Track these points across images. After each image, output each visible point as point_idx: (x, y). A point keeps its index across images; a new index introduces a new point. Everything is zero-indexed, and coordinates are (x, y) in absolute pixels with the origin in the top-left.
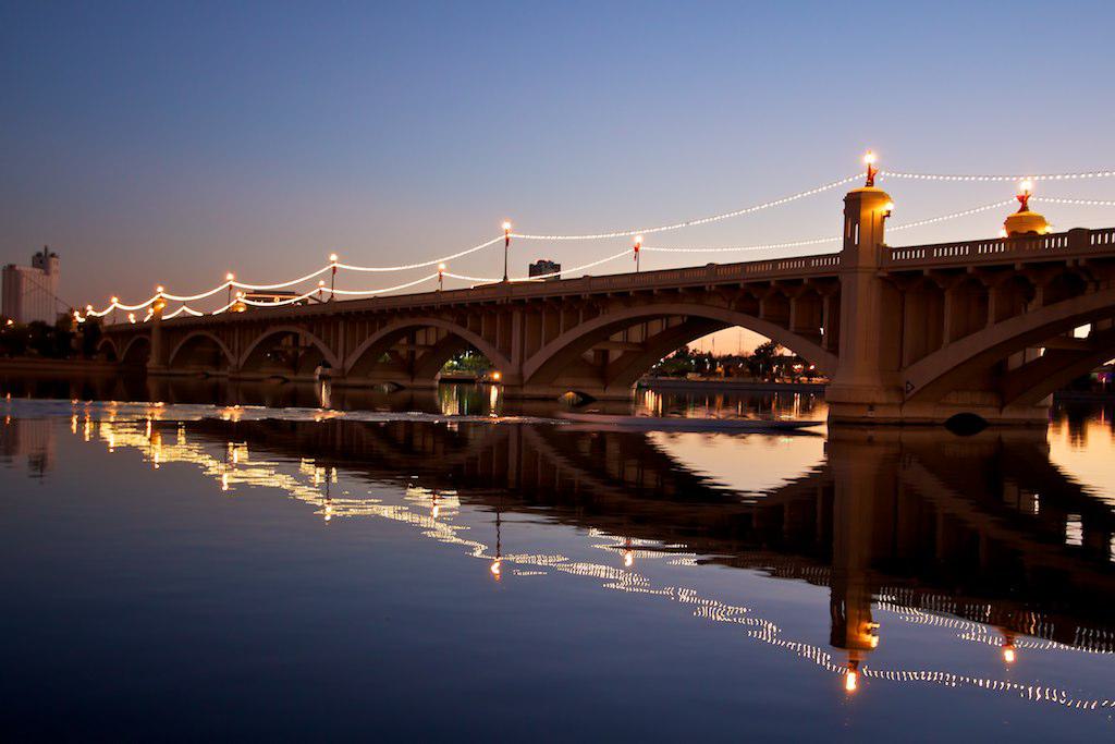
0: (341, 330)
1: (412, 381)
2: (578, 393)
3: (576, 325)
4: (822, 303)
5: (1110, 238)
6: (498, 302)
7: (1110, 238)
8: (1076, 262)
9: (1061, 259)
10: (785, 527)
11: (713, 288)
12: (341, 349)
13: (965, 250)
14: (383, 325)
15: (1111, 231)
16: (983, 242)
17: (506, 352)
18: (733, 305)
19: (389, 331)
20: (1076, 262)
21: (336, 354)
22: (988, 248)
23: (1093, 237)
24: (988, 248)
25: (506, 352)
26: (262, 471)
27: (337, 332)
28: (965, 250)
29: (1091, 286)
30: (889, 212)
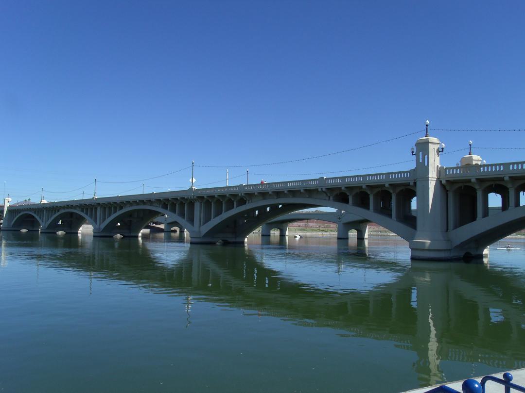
0: (45, 213)
1: (130, 233)
2: (223, 240)
3: (233, 208)
4: (211, 205)
5: (522, 166)
6: (320, 190)
7: (522, 166)
8: (322, 189)
9: (340, 186)
10: (183, 279)
11: (243, 195)
12: (44, 220)
13: (360, 179)
14: (58, 211)
15: (522, 163)
16: (369, 175)
17: (191, 220)
18: (331, 198)
19: (127, 211)
20: (322, 189)
21: (43, 221)
22: (350, 180)
23: (482, 168)
24: (350, 180)
25: (191, 220)
26: (335, 288)
27: (43, 213)
28: (360, 179)
29: (247, 202)
30: (443, 149)
